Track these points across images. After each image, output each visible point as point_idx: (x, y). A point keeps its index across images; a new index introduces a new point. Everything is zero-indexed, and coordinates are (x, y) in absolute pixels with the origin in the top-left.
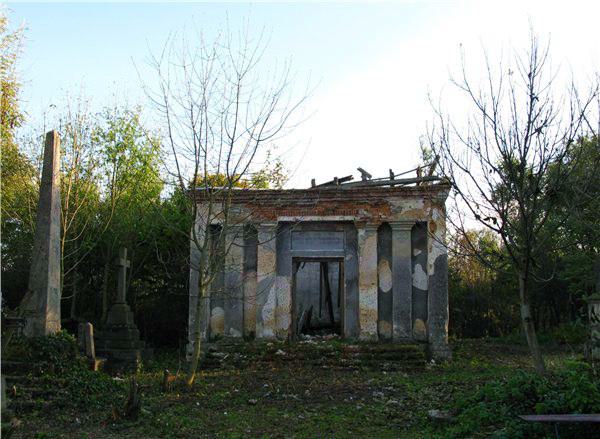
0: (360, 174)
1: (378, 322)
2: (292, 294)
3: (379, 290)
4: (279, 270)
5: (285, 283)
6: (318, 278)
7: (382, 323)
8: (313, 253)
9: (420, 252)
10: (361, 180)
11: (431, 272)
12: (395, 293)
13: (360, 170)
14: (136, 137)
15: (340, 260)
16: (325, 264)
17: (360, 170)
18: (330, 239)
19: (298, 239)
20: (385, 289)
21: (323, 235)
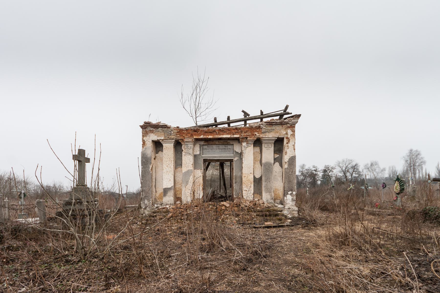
0: (243, 114)
1: (253, 194)
2: (242, 182)
3: (254, 177)
4: (196, 165)
5: (199, 173)
6: (219, 174)
7: (256, 195)
8: (215, 157)
9: (278, 156)
10: (227, 124)
11: (286, 166)
12: (263, 178)
13: (243, 111)
14: (131, 269)
15: (231, 161)
16: (222, 163)
17: (243, 111)
18: (225, 149)
19: (206, 149)
20: (258, 176)
21: (221, 147)
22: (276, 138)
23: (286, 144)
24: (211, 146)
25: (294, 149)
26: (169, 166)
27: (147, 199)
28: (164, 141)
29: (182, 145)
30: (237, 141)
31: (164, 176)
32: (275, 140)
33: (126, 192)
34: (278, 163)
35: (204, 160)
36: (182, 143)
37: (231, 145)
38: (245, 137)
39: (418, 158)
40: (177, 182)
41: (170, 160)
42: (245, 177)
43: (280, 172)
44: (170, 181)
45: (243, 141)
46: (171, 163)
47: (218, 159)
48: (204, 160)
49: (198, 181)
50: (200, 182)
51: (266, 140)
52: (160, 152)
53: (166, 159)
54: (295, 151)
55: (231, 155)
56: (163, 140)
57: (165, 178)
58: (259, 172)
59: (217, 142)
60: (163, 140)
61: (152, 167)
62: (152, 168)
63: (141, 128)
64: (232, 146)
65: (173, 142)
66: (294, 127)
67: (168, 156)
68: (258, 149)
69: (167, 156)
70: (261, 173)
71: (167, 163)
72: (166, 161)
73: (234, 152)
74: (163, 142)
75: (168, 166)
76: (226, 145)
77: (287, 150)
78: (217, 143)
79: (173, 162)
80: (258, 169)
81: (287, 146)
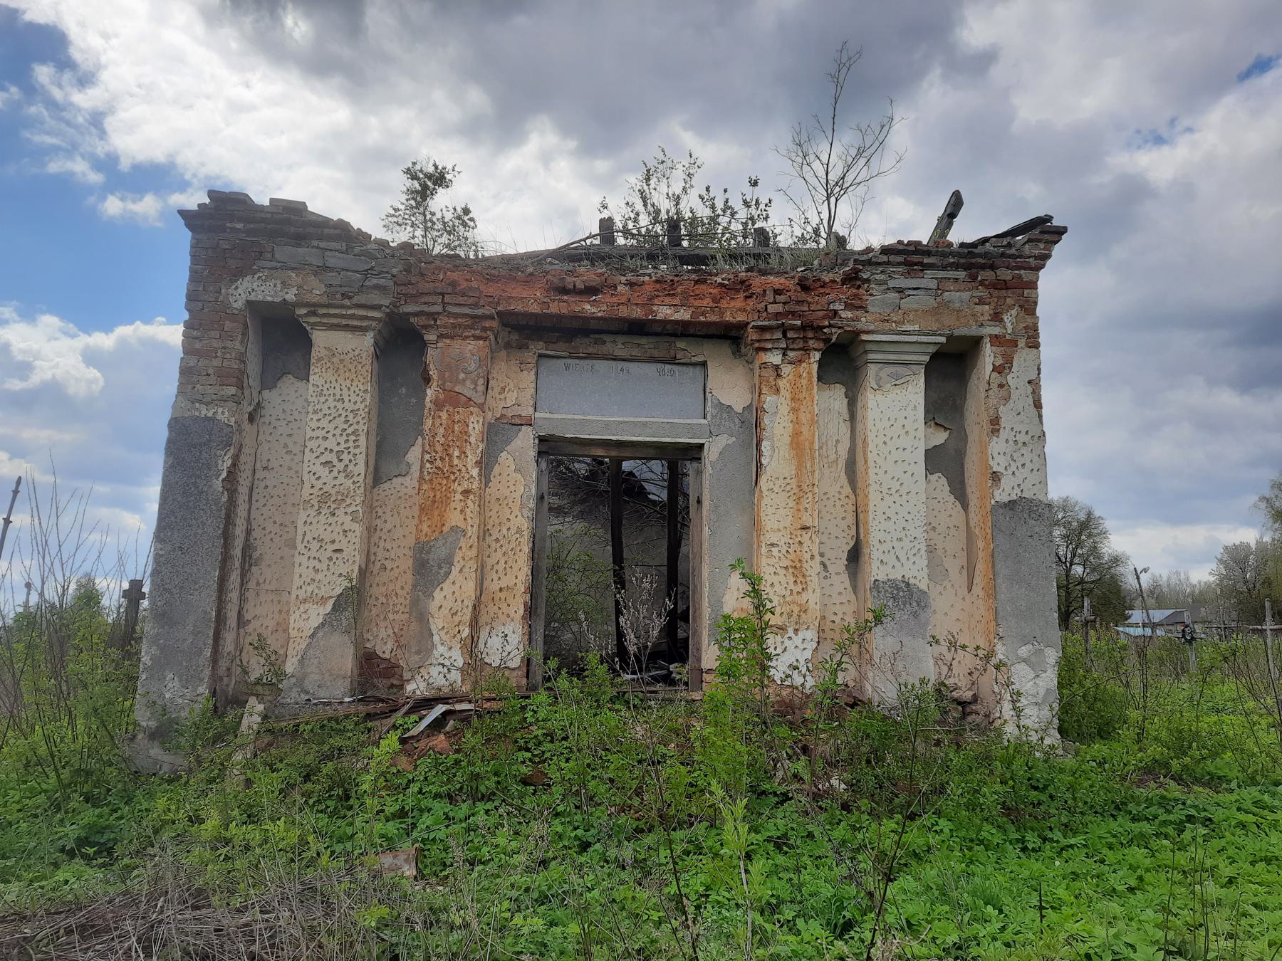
22: (943, 340)
23: (995, 374)
24: (583, 362)
25: (1038, 405)
26: (341, 466)
27: (763, 661)
28: (322, 311)
29: (424, 345)
30: (726, 348)
31: (300, 523)
32: (932, 349)
33: (541, 369)
34: (944, 481)
35: (542, 440)
36: (430, 337)
37: (694, 364)
38: (778, 327)
39: (347, 632)
40: (378, 565)
41: (350, 430)
42: (775, 550)
43: (953, 531)
44: (335, 556)
45: (762, 345)
46: (351, 444)
47: (635, 439)
48: (542, 440)
49: (502, 565)
50: (515, 567)
51: (887, 347)
52: (289, 379)
53: (324, 423)
54: (1040, 416)
55: (695, 421)
56: (313, 309)
57: (308, 537)
58: (843, 525)
59: (620, 346)
60: (314, 305)
61: (234, 465)
62: (229, 473)
63: (188, 226)
64: (698, 370)
65: (374, 324)
66: (1033, 285)
67: (340, 405)
68: (835, 398)
69: (331, 403)
70: (854, 532)
71: (331, 444)
72: (321, 433)
73: (709, 404)
74: (313, 319)
75: (335, 461)
76: (668, 367)
77: (1001, 408)
78: (620, 351)
79: (363, 440)
80: (838, 504)
81: (1001, 386)
